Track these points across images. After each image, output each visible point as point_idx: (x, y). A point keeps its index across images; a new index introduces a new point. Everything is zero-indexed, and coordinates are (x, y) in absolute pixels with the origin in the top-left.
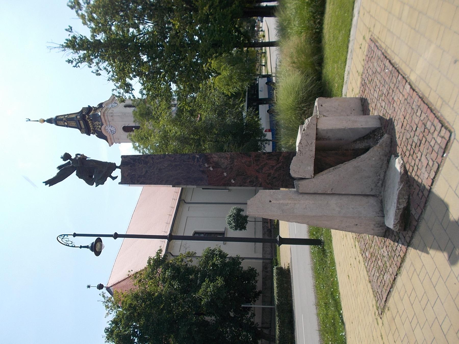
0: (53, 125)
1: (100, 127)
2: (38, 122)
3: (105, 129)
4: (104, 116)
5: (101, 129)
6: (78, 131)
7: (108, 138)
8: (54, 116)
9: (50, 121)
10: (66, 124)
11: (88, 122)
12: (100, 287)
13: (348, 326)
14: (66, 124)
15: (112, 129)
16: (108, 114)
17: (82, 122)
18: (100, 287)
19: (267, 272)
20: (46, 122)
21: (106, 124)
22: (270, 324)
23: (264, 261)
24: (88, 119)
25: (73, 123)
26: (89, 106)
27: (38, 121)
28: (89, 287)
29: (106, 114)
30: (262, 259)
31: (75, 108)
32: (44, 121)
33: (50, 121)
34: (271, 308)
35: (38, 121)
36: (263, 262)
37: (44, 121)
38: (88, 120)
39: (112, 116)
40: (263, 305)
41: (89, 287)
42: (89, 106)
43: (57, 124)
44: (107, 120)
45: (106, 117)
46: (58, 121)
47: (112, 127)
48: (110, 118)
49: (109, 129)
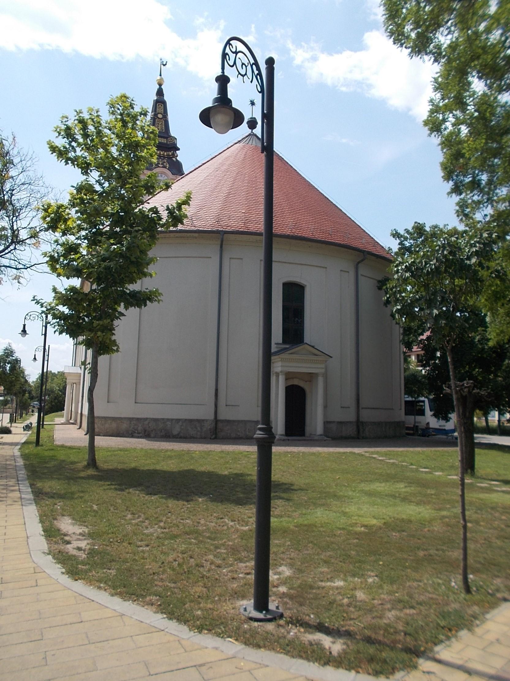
9: (160, 93)
20: (158, 87)
32: (160, 85)
33: (160, 93)
35: (161, 75)
37: (160, 85)
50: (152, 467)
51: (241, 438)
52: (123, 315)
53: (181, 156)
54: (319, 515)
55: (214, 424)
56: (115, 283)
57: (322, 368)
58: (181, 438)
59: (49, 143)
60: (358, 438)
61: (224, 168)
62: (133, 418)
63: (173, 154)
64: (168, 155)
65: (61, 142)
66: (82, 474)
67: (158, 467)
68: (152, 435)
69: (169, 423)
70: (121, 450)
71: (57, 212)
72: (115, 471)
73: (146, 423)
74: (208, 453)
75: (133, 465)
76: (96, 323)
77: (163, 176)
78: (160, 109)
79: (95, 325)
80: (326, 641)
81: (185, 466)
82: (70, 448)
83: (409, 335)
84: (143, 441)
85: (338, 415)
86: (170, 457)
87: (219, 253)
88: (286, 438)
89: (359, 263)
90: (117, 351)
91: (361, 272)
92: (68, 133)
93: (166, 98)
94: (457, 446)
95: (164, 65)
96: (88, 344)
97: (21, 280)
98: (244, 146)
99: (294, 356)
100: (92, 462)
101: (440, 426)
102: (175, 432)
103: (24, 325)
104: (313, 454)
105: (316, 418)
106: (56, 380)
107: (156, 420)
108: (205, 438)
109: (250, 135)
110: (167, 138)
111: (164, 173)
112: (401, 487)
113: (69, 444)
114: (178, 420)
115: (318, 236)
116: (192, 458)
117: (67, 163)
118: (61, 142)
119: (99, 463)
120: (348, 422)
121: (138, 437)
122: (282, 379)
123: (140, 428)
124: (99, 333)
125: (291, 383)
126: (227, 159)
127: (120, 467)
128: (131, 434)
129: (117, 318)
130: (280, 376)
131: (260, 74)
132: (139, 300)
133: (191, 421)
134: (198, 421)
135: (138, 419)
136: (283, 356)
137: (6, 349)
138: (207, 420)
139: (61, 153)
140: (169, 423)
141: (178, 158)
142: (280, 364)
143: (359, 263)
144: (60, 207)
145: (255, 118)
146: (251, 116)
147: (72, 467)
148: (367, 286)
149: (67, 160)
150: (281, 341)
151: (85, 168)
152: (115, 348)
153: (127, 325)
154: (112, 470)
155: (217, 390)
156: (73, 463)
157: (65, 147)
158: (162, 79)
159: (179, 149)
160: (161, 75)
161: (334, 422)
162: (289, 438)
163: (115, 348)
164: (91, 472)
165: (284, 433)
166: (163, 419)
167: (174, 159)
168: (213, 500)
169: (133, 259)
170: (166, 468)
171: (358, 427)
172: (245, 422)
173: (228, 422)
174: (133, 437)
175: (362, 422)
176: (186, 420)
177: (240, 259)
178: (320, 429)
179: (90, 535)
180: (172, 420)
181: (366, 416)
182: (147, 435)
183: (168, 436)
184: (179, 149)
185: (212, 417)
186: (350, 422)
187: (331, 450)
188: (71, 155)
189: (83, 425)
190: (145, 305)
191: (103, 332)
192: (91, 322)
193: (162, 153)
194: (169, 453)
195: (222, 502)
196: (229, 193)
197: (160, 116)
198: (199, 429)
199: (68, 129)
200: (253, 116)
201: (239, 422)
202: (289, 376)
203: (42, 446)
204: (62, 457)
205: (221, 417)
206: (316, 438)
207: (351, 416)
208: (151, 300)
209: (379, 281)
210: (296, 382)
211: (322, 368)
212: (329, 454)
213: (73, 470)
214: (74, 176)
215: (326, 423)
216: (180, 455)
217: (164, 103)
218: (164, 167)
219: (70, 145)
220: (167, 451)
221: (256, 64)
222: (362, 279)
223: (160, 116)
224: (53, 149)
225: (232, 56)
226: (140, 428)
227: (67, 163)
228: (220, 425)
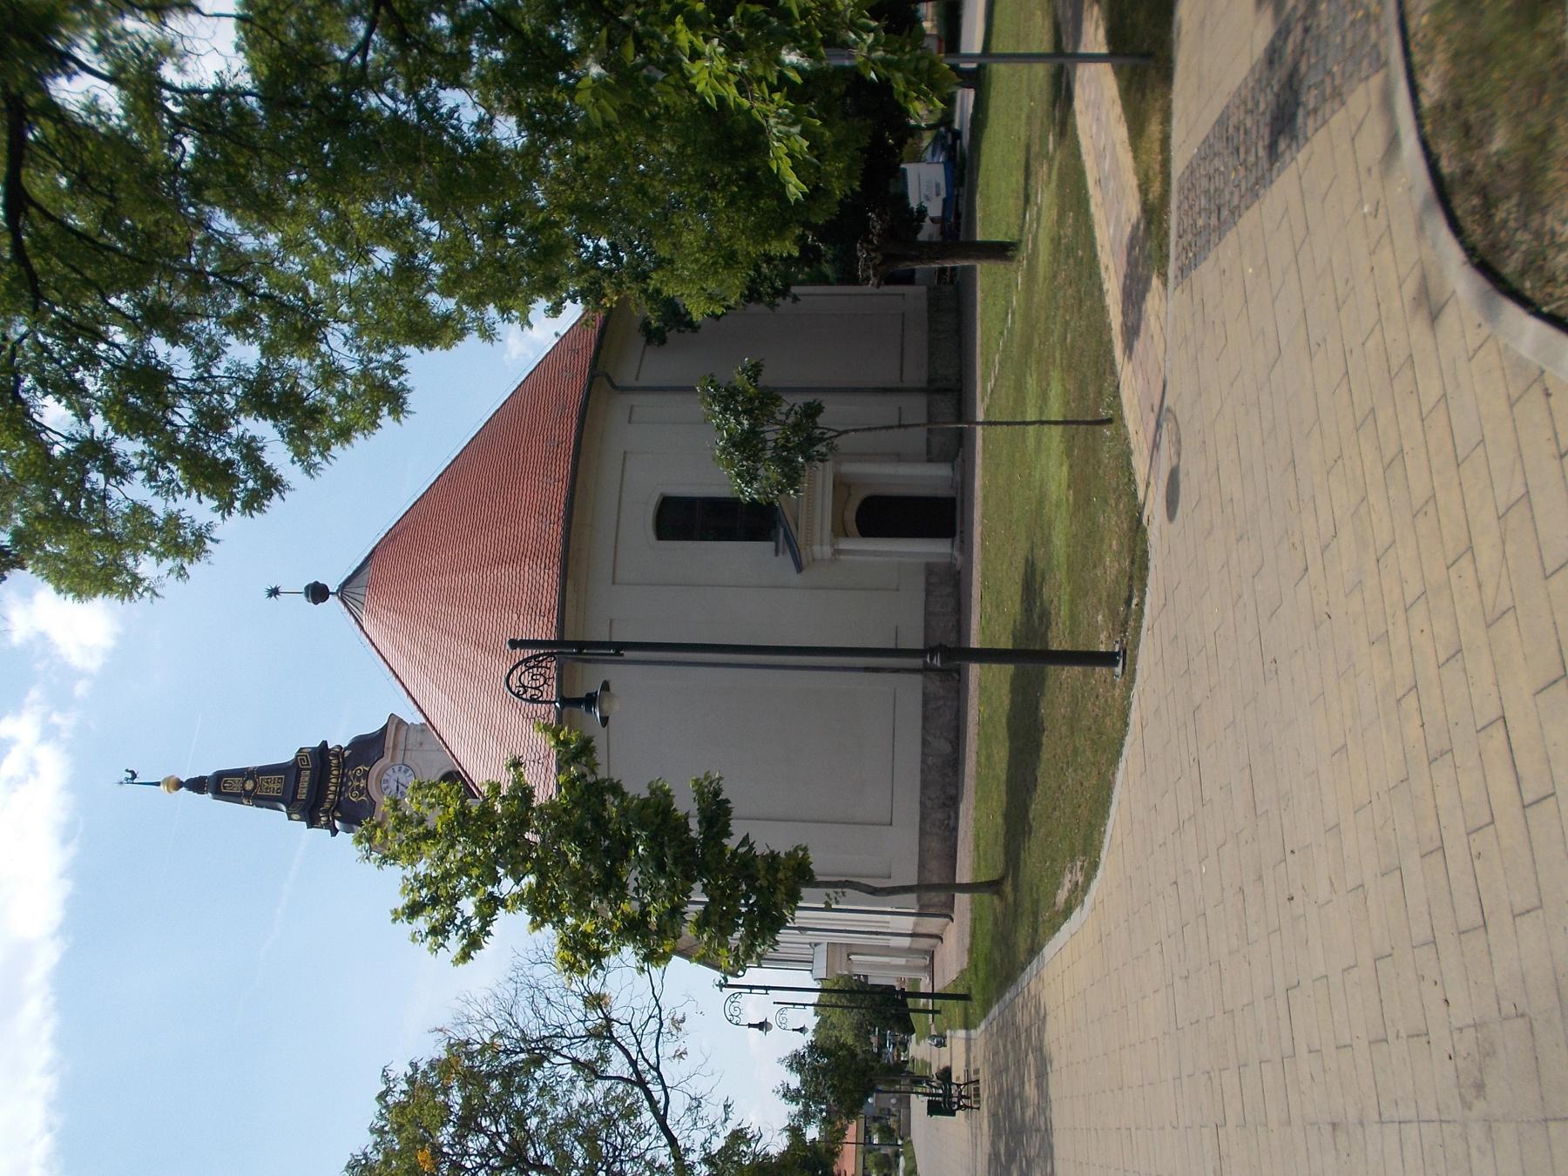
3: (379, 780)
9: (197, 785)
12: (317, 593)
18: (317, 593)
28: (274, 592)
32: (179, 785)
33: (197, 785)
35: (158, 784)
37: (179, 785)
46: (219, 785)
50: (1003, 788)
51: (959, 622)
52: (746, 839)
53: (340, 738)
54: (1059, 540)
55: (932, 675)
56: (692, 852)
58: (957, 738)
59: (456, 962)
60: (960, 390)
61: (418, 652)
62: (921, 829)
63: (336, 755)
64: (338, 766)
65: (455, 943)
66: (1011, 898)
67: (1004, 777)
68: (953, 792)
69: (930, 760)
70: (977, 846)
71: (574, 950)
72: (1007, 847)
73: (929, 804)
74: (983, 689)
75: (1000, 820)
76: (762, 882)
78: (235, 785)
79: (765, 884)
80: (1135, 601)
81: (1002, 733)
82: (973, 935)
83: (759, 294)
84: (962, 807)
85: (916, 439)
86: (989, 757)
87: (591, 666)
88: (958, 538)
89: (613, 386)
90: (805, 849)
91: (629, 380)
92: (438, 931)
93: (208, 772)
94: (973, 268)
95: (134, 776)
96: (793, 897)
97: (679, 1017)
98: (369, 611)
99: (802, 522)
100: (993, 886)
102: (946, 748)
103: (750, 1025)
104: (985, 498)
105: (922, 477)
106: (834, 1020)
107: (924, 786)
108: (958, 692)
109: (342, 599)
110: (299, 771)
111: (380, 774)
112: (1031, 382)
113: (967, 941)
114: (925, 743)
115: (564, 469)
116: (990, 718)
117: (489, 934)
118: (455, 943)
119: (993, 875)
121: (957, 818)
122: (845, 544)
123: (940, 816)
124: (780, 875)
125: (852, 526)
126: (400, 649)
127: (1001, 840)
128: (951, 832)
129: (751, 848)
130: (841, 547)
131: (535, 657)
132: (716, 813)
133: (925, 718)
134: (925, 703)
135: (923, 819)
136: (801, 541)
137: (791, 1066)
138: (925, 688)
139: (473, 943)
140: (930, 760)
141: (344, 745)
142: (816, 548)
143: (613, 386)
144: (564, 945)
145: (307, 588)
147: (1000, 917)
148: (659, 366)
149: (484, 930)
150: (772, 544)
151: (491, 905)
152: (801, 854)
153: (759, 830)
154: (1007, 853)
156: (995, 924)
157: (463, 937)
158: (167, 782)
159: (325, 744)
160: (158, 784)
162: (958, 530)
163: (801, 854)
164: (1008, 888)
165: (949, 541)
166: (922, 771)
167: (347, 753)
168: (1042, 694)
169: (658, 820)
170: (1004, 765)
171: (939, 391)
172: (928, 614)
174: (955, 829)
175: (930, 381)
176: (924, 728)
178: (941, 471)
179: (1072, 860)
180: (923, 753)
181: (917, 374)
182: (952, 802)
183: (954, 763)
184: (325, 744)
185: (919, 678)
186: (929, 406)
187: (979, 472)
188: (475, 924)
189: (935, 931)
190: (728, 801)
191: (777, 870)
192: (759, 891)
194: (983, 759)
195: (1044, 679)
196: (477, 644)
197: (249, 785)
198: (941, 703)
199: (434, 931)
201: (927, 627)
202: (840, 531)
203: (969, 989)
204: (988, 943)
206: (958, 478)
207: (916, 407)
208: (717, 793)
209: (649, 342)
210: (851, 516)
212: (985, 469)
213: (1005, 916)
214: (512, 926)
215: (931, 459)
216: (986, 740)
217: (220, 776)
218: (366, 775)
219: (460, 927)
220: (978, 763)
221: (526, 661)
222: (647, 379)
223: (249, 785)
224: (465, 956)
225: (530, 692)
226: (940, 816)
227: (489, 934)
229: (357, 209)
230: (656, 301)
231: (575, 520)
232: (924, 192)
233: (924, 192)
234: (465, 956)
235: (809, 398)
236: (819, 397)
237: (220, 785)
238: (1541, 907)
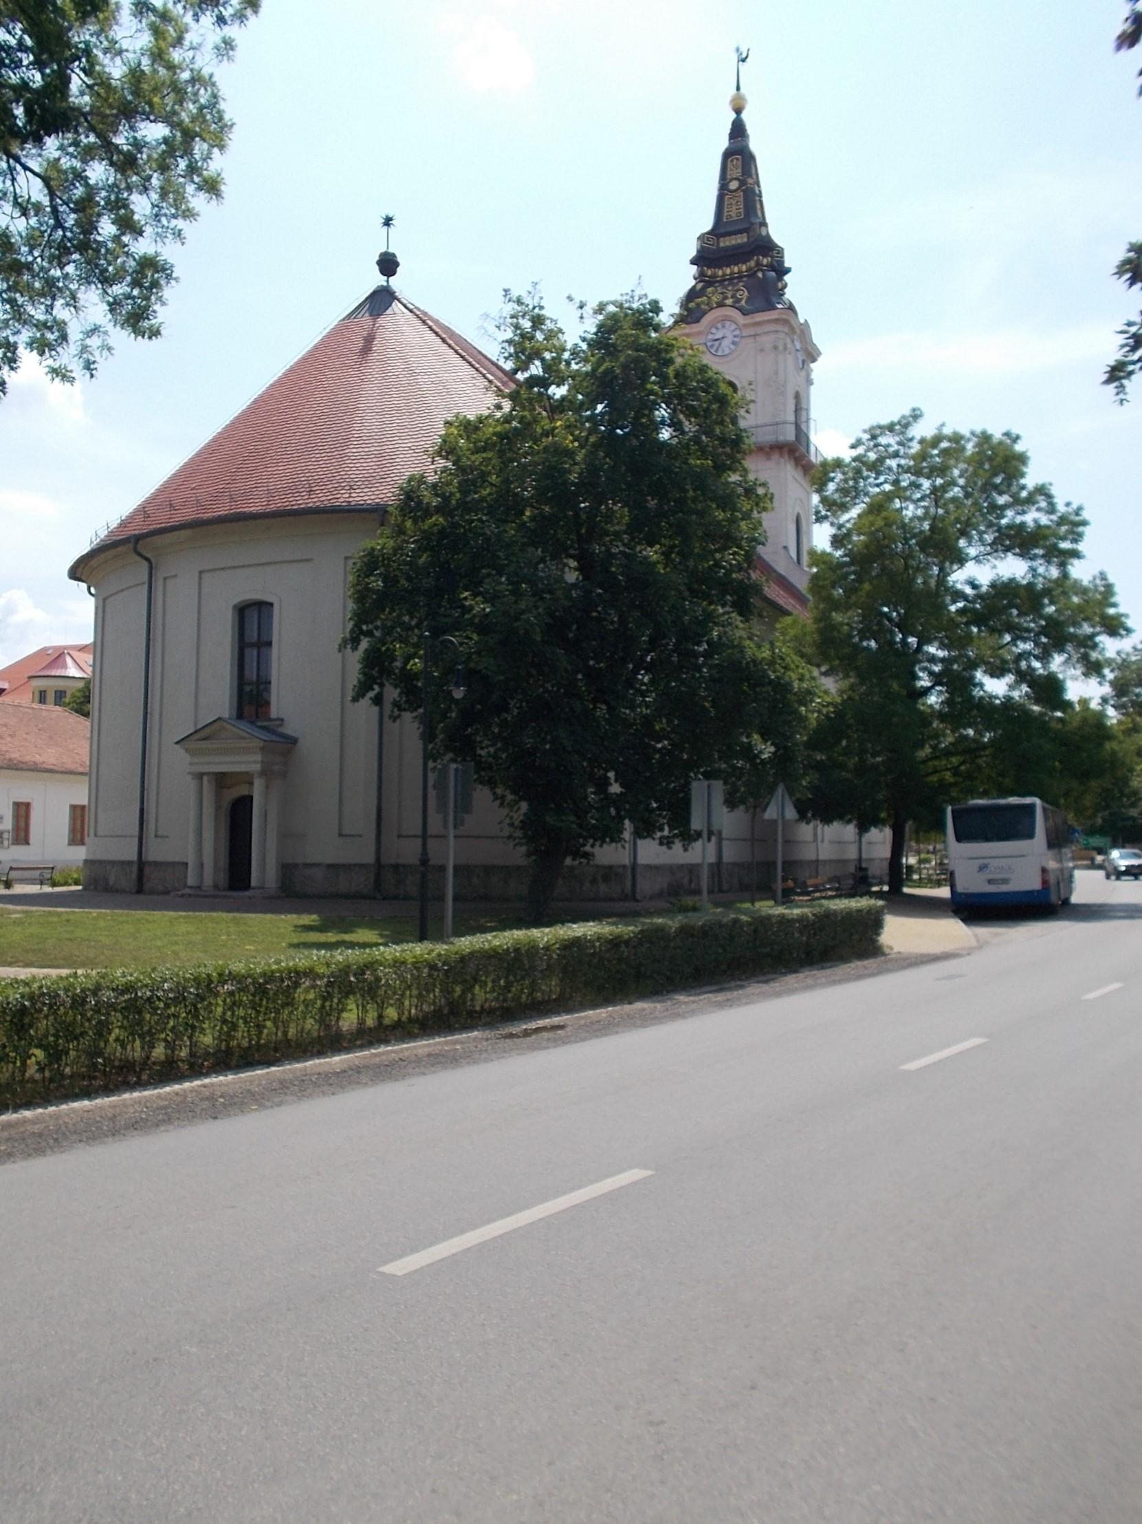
0: (724, 143)
1: (729, 301)
2: (734, 91)
3: (726, 319)
4: (776, 321)
5: (721, 305)
6: (707, 224)
7: (695, 328)
8: (754, 145)
9: (738, 131)
10: (734, 185)
11: (744, 262)
12: (388, 265)
13: (24, 1163)
14: (734, 185)
15: (725, 343)
16: (781, 336)
17: (741, 239)
18: (388, 265)
19: (594, 881)
20: (734, 116)
21: (745, 326)
22: (396, 897)
23: (629, 872)
24: (758, 264)
25: (735, 211)
26: (693, 262)
27: (738, 89)
28: (388, 222)
29: (779, 327)
30: (634, 865)
31: (780, 224)
32: (738, 111)
33: (738, 131)
34: (455, 899)
35: (738, 89)
36: (624, 866)
37: (738, 111)
38: (752, 263)
39: (776, 348)
40: (456, 868)
41: (388, 222)
42: (693, 262)
43: (727, 155)
44: (759, 330)
45: (773, 327)
46: (738, 158)
47: (734, 343)
48: (767, 341)
49: (727, 333)
57: (255, 762)
77: (728, 324)
101: (990, 882)
114: (113, 863)
120: (355, 865)
146: (384, 250)
155: (142, 811)
161: (319, 865)
173: (156, 864)
177: (307, 560)
193: (736, 269)
200: (390, 251)
205: (152, 854)
207: (129, 853)
211: (255, 762)
228: (147, 870)
229: (922, 846)
230: (1110, 869)
231: (234, 524)
232: (994, 863)
233: (994, 863)
234: (916, 415)
235: (982, 861)
236: (986, 861)
237: (738, 158)
238: (340, 835)
